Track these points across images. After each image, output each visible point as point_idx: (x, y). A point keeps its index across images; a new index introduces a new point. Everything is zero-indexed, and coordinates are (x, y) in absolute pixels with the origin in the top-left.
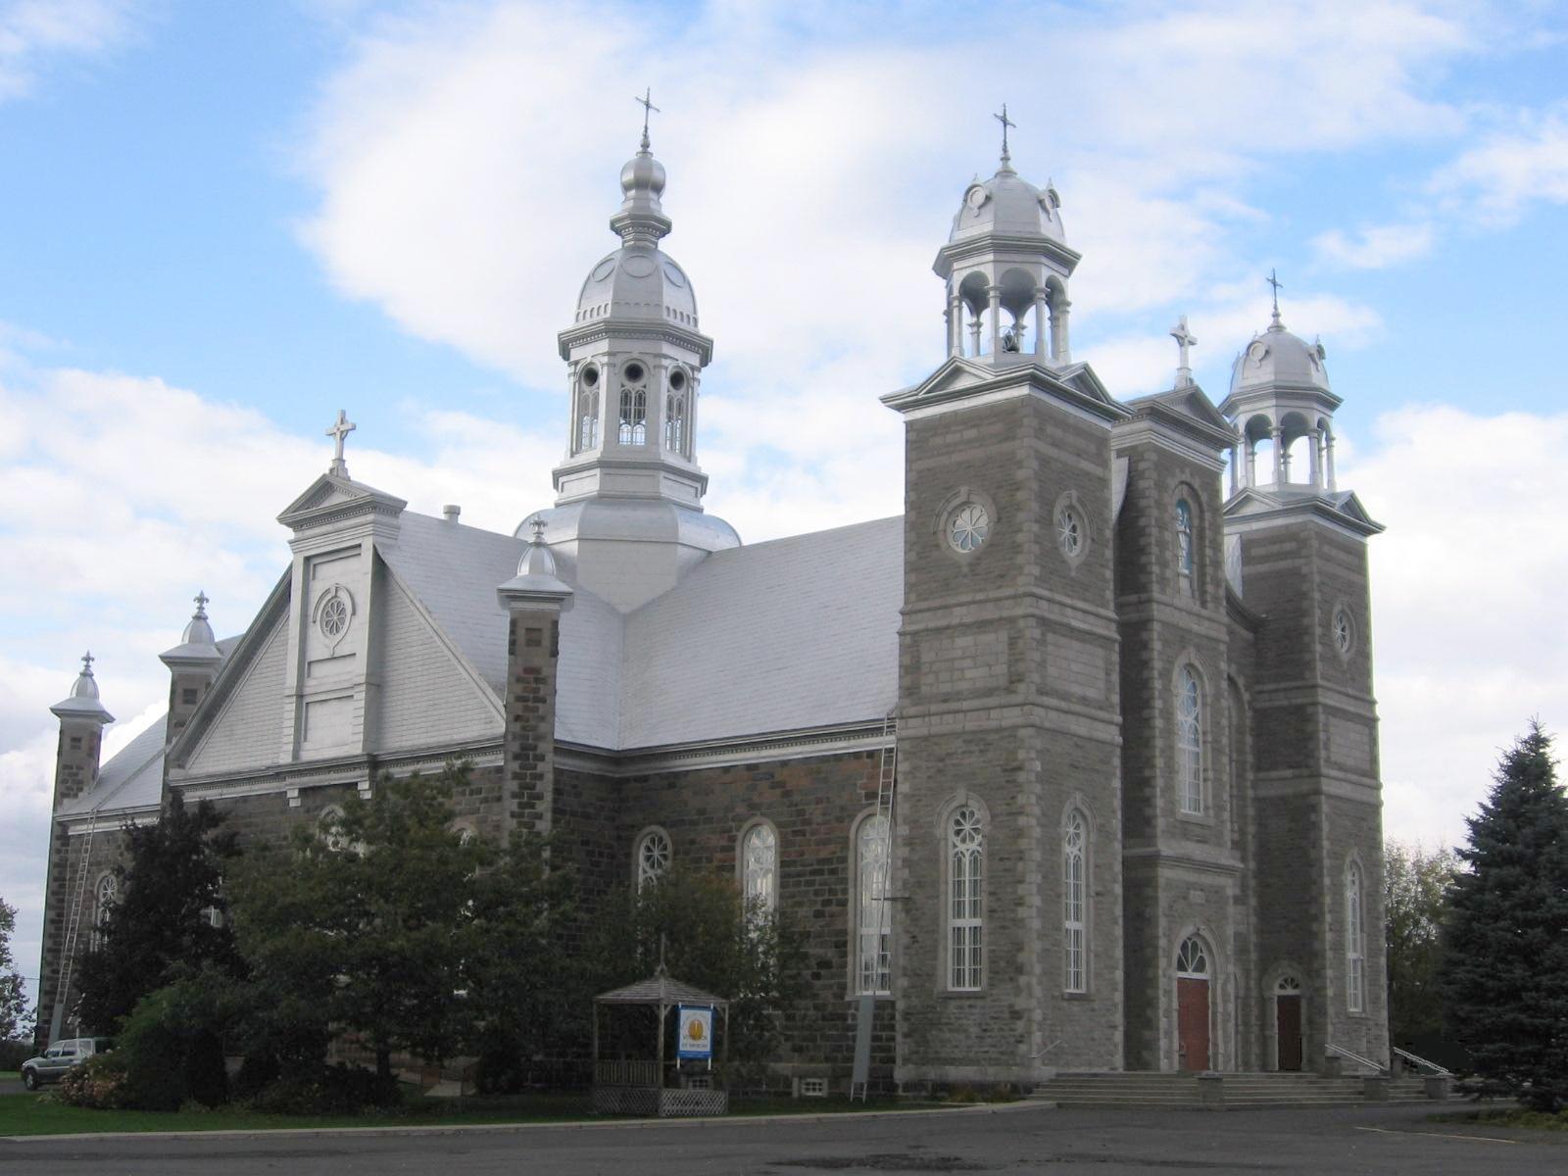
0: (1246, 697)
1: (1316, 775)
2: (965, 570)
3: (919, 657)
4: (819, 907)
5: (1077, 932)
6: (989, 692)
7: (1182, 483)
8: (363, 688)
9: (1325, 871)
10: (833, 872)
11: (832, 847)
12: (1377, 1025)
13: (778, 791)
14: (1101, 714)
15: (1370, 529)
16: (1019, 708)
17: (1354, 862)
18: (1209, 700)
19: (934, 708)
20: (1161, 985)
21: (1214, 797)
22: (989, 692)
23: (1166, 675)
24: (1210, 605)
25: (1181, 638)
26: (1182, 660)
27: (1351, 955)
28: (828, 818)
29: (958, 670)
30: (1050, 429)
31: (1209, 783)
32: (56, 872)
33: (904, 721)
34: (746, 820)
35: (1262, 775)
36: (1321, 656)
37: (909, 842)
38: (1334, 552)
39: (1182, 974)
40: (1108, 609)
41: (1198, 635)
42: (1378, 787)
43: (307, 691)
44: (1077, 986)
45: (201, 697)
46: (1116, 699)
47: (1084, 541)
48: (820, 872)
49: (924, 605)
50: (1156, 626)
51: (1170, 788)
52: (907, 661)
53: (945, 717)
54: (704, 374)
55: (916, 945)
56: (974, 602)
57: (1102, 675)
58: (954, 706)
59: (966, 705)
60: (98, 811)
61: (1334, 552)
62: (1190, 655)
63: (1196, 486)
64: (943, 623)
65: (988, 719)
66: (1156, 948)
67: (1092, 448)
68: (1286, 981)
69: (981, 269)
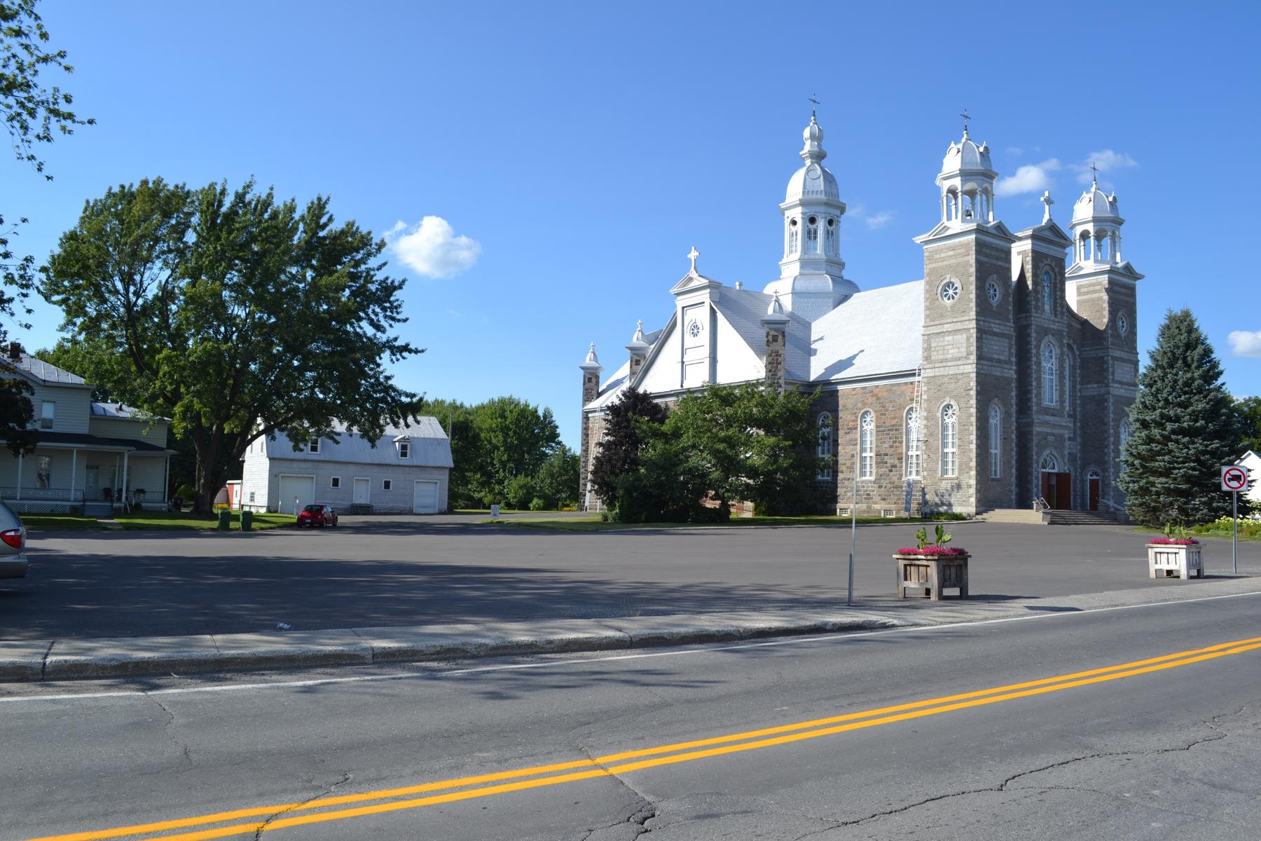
1: (1107, 386)
2: (949, 309)
6: (959, 359)
10: (897, 430)
11: (896, 420)
13: (874, 398)
15: (1138, 277)
22: (959, 359)
23: (1038, 347)
25: (1045, 331)
30: (984, 250)
37: (927, 418)
38: (1119, 289)
43: (684, 360)
45: (642, 363)
46: (1013, 359)
48: (892, 430)
50: (1034, 327)
51: (1039, 394)
52: (925, 346)
57: (1007, 350)
58: (944, 364)
61: (1119, 289)
62: (1050, 338)
64: (940, 331)
67: (1003, 256)
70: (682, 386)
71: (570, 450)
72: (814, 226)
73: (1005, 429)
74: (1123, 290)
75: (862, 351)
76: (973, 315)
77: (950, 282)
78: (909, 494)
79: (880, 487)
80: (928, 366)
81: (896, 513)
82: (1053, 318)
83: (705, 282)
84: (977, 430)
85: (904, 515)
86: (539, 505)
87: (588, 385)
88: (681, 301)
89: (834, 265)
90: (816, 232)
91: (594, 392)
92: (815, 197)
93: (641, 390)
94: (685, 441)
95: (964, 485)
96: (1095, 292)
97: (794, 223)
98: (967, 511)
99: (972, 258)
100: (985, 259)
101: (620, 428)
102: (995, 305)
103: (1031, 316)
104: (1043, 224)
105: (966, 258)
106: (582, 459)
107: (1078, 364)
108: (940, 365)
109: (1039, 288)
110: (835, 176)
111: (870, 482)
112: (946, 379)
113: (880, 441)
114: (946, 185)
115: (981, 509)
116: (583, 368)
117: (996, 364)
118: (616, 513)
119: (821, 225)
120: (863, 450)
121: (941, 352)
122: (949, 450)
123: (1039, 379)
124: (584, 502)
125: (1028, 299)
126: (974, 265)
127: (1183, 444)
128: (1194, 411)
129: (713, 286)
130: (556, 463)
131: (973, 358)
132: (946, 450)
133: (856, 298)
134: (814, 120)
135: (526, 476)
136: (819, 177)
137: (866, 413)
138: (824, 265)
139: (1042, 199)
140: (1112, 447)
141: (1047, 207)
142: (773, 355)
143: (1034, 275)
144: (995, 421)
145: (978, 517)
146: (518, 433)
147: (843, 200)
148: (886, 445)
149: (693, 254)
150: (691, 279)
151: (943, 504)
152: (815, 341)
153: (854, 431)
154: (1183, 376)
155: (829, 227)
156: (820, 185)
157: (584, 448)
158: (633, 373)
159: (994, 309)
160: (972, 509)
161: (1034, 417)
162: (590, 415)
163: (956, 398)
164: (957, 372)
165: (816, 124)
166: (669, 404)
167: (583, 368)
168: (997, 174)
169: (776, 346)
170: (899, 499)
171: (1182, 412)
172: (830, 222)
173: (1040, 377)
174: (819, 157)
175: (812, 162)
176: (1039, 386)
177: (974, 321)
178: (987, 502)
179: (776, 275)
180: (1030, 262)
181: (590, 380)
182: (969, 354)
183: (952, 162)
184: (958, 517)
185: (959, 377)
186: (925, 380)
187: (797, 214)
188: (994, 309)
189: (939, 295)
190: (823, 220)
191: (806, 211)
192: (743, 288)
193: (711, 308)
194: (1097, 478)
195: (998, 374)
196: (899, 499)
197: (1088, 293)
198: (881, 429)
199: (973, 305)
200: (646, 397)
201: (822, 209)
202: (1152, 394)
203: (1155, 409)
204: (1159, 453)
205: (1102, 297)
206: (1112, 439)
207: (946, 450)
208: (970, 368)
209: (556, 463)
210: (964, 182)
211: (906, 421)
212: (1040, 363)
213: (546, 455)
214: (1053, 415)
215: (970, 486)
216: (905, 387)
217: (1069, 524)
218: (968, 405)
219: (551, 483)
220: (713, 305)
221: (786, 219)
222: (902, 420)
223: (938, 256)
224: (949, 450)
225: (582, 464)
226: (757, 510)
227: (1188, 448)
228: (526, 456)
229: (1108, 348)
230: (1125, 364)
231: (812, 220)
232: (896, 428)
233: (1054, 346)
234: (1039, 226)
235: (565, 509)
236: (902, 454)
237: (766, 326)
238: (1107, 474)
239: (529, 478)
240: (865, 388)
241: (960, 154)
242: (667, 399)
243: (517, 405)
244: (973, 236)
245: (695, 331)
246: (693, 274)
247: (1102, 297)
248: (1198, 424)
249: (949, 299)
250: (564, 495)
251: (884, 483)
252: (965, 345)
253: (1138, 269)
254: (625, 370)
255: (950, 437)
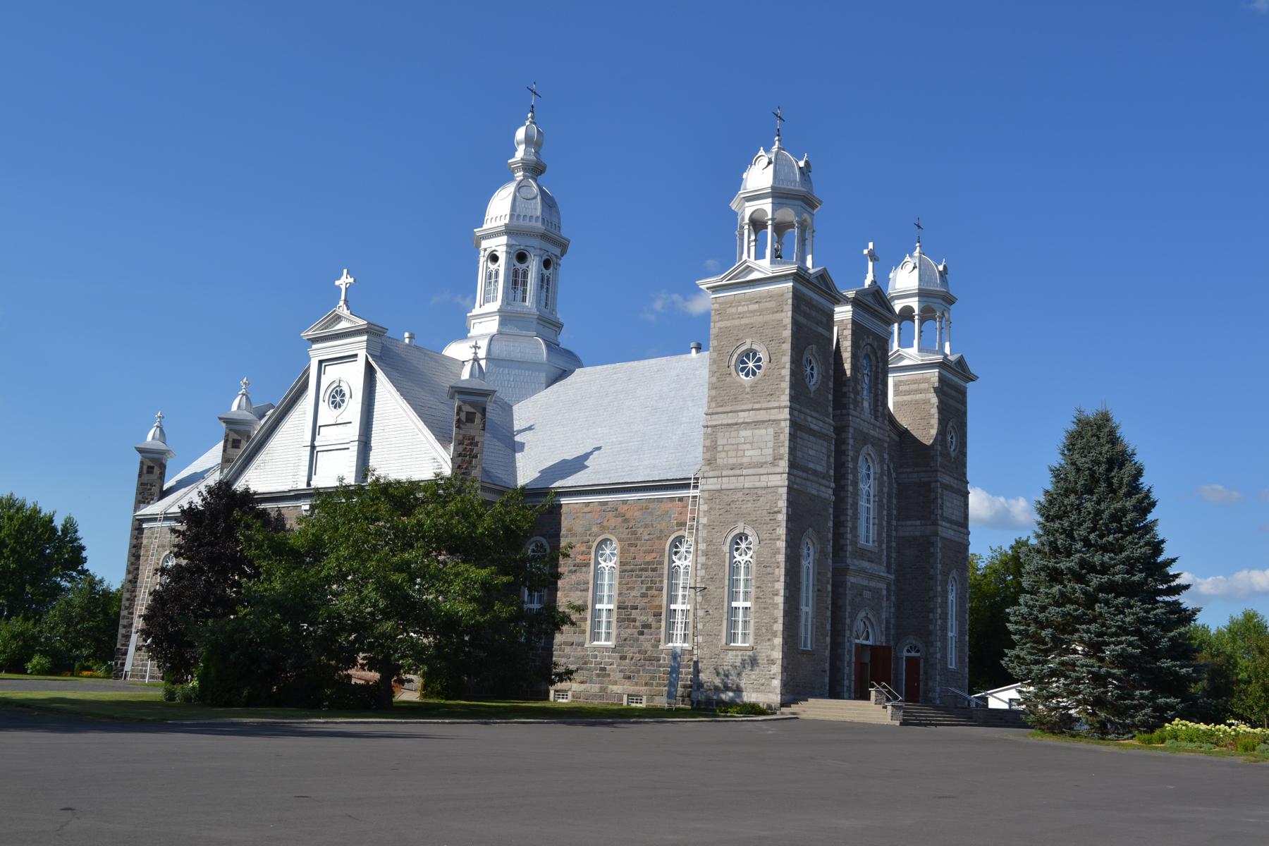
0: (894, 475)
1: (935, 523)
2: (748, 390)
3: (716, 441)
4: (644, 591)
5: (807, 613)
6: (762, 465)
7: (868, 344)
8: (357, 443)
9: (938, 582)
10: (654, 570)
11: (654, 555)
12: (963, 677)
13: (620, 519)
14: (824, 482)
15: (970, 378)
16: (780, 475)
17: (954, 577)
18: (877, 476)
19: (725, 473)
20: (846, 647)
21: (878, 534)
22: (762, 465)
23: (855, 459)
24: (880, 419)
25: (864, 439)
26: (864, 451)
27: (950, 634)
28: (651, 536)
29: (741, 450)
30: (803, 307)
31: (876, 526)
32: (134, 550)
33: (705, 480)
34: (599, 536)
35: (900, 523)
36: (940, 453)
37: (706, 554)
38: (950, 391)
39: (857, 641)
40: (829, 418)
41: (873, 437)
42: (968, 533)
43: (316, 444)
44: (744, 642)
45: (244, 445)
46: (832, 472)
47: (818, 376)
48: (646, 570)
49: (720, 410)
50: (851, 430)
51: (855, 528)
52: (708, 443)
53: (731, 478)
54: (563, 261)
55: (708, 616)
56: (752, 410)
57: (825, 458)
58: (738, 472)
59: (745, 472)
60: (165, 513)
61: (950, 391)
62: (868, 448)
63: (875, 346)
64: (733, 421)
65: (760, 481)
66: (845, 624)
67: (824, 320)
68: (911, 647)
69: (763, 207)
70: (309, 484)
71: (101, 581)
72: (524, 266)
73: (819, 575)
74: (954, 393)
75: (599, 448)
76: (785, 399)
77: (751, 350)
78: (675, 670)
79: (623, 658)
80: (711, 474)
81: (648, 700)
82: (873, 421)
83: (361, 323)
84: (786, 575)
85: (661, 702)
86: (42, 665)
87: (146, 478)
88: (318, 353)
89: (549, 325)
90: (525, 274)
91: (155, 490)
92: (527, 223)
93: (239, 486)
94: (330, 565)
95: (762, 659)
96: (920, 391)
97: (494, 258)
98: (767, 701)
99: (787, 316)
100: (804, 321)
101: (200, 546)
102: (813, 389)
103: (849, 414)
104: (866, 286)
105: (778, 316)
106: (126, 595)
107: (894, 491)
108: (731, 472)
109: (859, 376)
110: (556, 200)
111: (607, 648)
112: (740, 494)
113: (625, 587)
114: (749, 209)
115: (788, 697)
116: (140, 450)
117: (810, 477)
118: (194, 688)
119: (533, 267)
120: (597, 599)
121: (732, 454)
122: (740, 604)
123: (855, 505)
124: (123, 665)
125: (845, 389)
126: (789, 327)
127: (1117, 607)
128: (1128, 558)
129: (374, 333)
130: (77, 601)
131: (784, 465)
132: (734, 604)
133: (579, 375)
134: (532, 118)
135: (26, 619)
136: (535, 198)
137: (605, 541)
138: (535, 322)
139: (866, 252)
140: (939, 611)
141: (870, 264)
142: (466, 442)
143: (854, 356)
144: (808, 563)
145: (783, 709)
146: (18, 552)
147: (565, 233)
148: (633, 593)
149: (344, 281)
150: (338, 318)
151: (727, 688)
152: (520, 432)
153: (584, 569)
154: (1109, 507)
155: (545, 271)
156: (536, 209)
157: (130, 577)
158: (226, 460)
159: (812, 396)
160: (775, 698)
161: (849, 560)
162: (144, 526)
163: (754, 523)
164: (758, 484)
165: (535, 123)
166: (283, 511)
167: (140, 450)
168: (820, 202)
169: (473, 430)
170: (653, 678)
171: (1111, 559)
172: (547, 264)
173: (857, 504)
174: (535, 169)
175: (524, 176)
176: (855, 517)
177: (787, 410)
178: (795, 691)
179: (462, 333)
180: (849, 337)
181: (150, 470)
182: (777, 458)
183: (759, 176)
184: (753, 709)
185: (760, 492)
186: (706, 495)
187: (499, 245)
188: (812, 396)
189: (733, 368)
190: (537, 259)
191: (514, 242)
192: (414, 343)
193: (368, 364)
194: (918, 655)
195: (814, 492)
196: (653, 678)
197: (909, 393)
198: (628, 568)
199: (786, 385)
200: (248, 498)
201: (537, 243)
202: (1065, 530)
203: (1069, 554)
204: (1079, 620)
205: (929, 399)
206: (939, 600)
207: (734, 604)
208: (778, 480)
209: (77, 601)
210: (776, 207)
211: (670, 557)
212: (857, 483)
213: (59, 588)
214: (871, 561)
215: (772, 662)
216: (670, 505)
217: (925, 725)
218: (774, 536)
219: (67, 632)
220: (370, 359)
221: (482, 253)
222: (662, 555)
223: (734, 310)
224: (740, 604)
225: (124, 602)
226: (426, 689)
227: (1123, 613)
228: (28, 588)
229: (937, 471)
230: (954, 495)
231: (522, 257)
232: (654, 567)
233: (873, 462)
234: (861, 288)
235: (85, 673)
236: (660, 607)
237: (457, 396)
238: (931, 650)
239: (32, 622)
240: (606, 503)
241: (771, 166)
242: (281, 505)
243: (21, 508)
244: (790, 284)
245: (338, 399)
246: (343, 310)
247: (929, 399)
248: (1136, 578)
249: (747, 375)
250: (85, 652)
251: (629, 651)
252: (771, 444)
253: (973, 368)
254: (214, 455)
255: (606, 588)
